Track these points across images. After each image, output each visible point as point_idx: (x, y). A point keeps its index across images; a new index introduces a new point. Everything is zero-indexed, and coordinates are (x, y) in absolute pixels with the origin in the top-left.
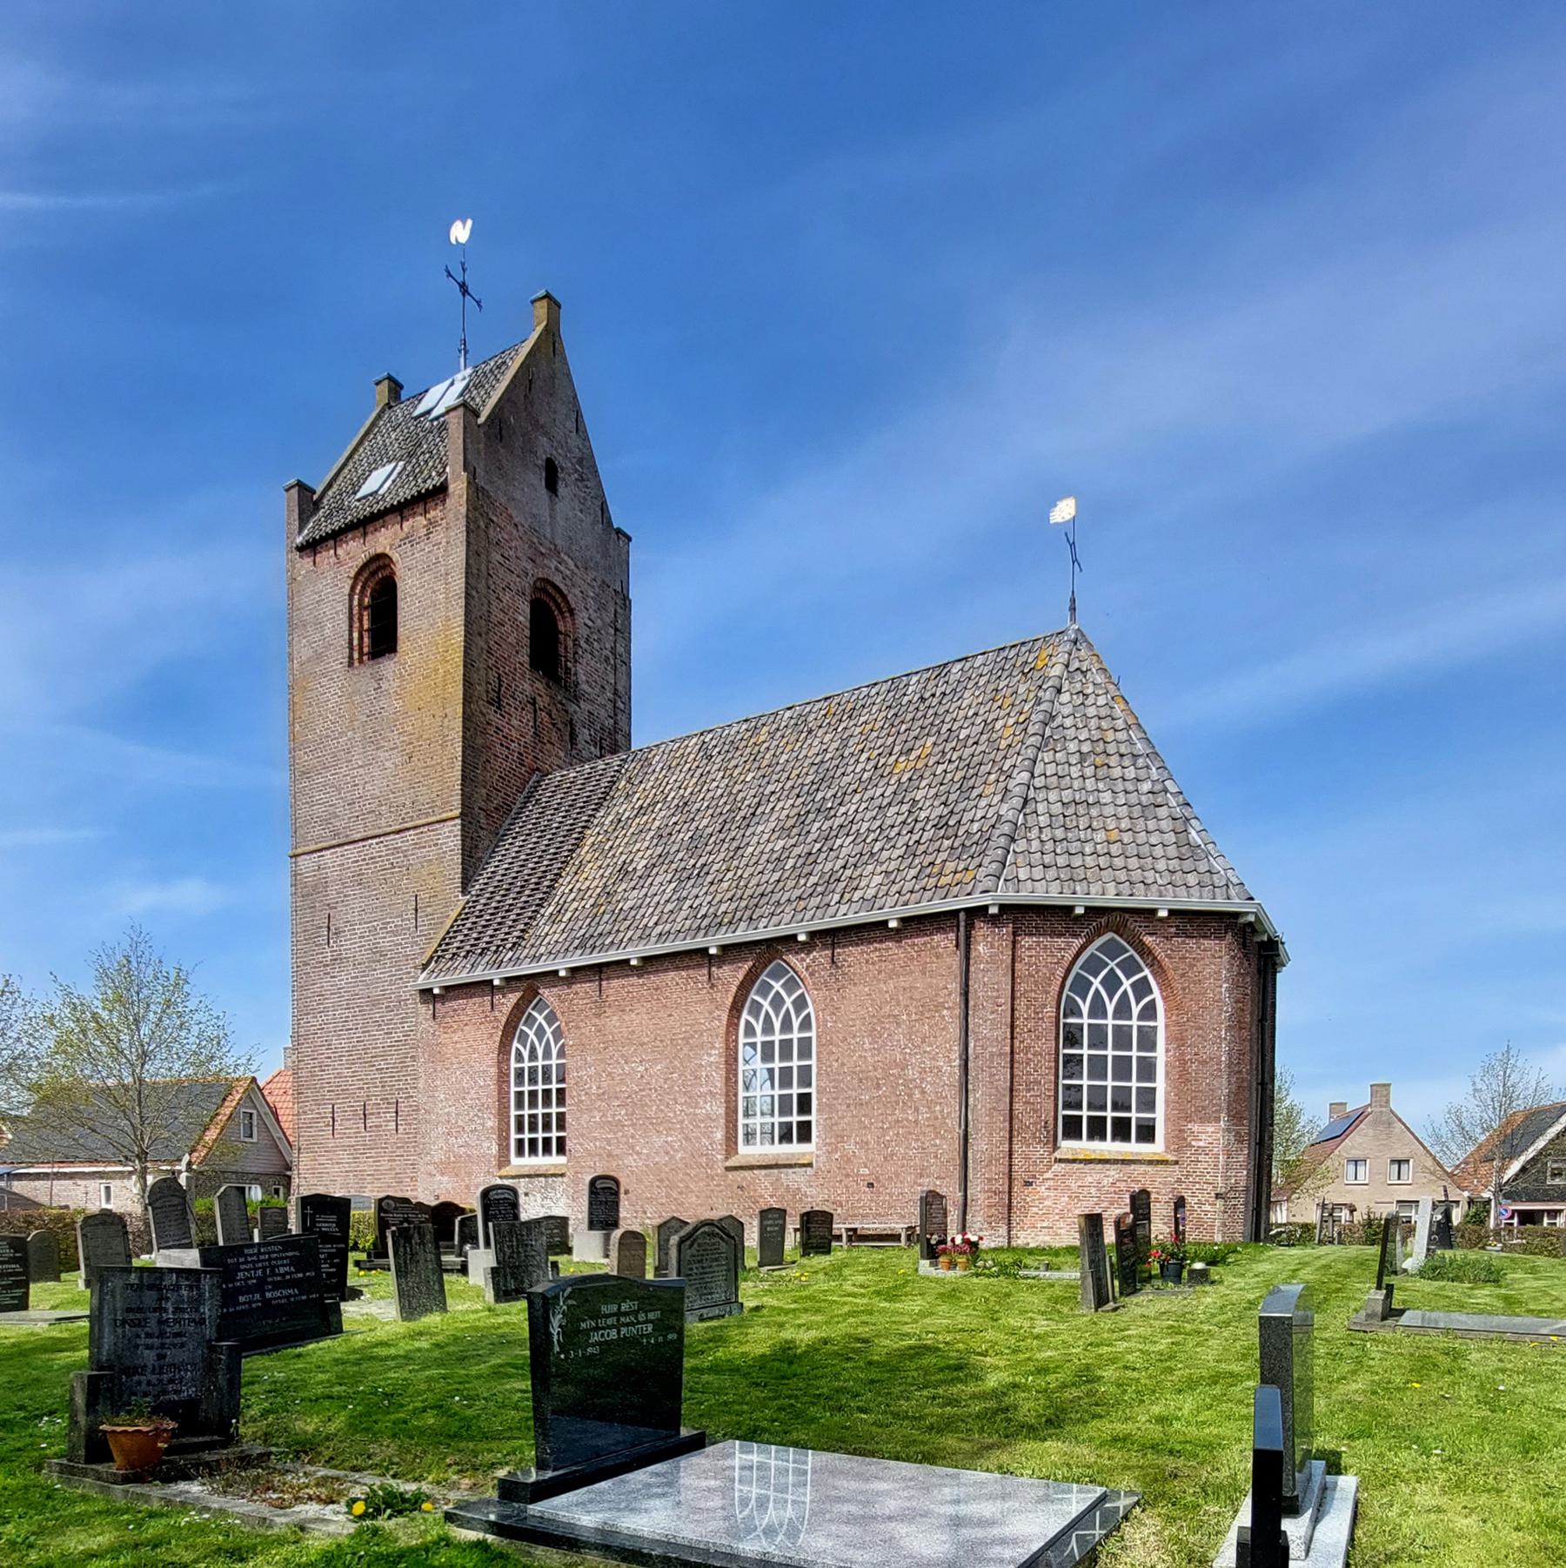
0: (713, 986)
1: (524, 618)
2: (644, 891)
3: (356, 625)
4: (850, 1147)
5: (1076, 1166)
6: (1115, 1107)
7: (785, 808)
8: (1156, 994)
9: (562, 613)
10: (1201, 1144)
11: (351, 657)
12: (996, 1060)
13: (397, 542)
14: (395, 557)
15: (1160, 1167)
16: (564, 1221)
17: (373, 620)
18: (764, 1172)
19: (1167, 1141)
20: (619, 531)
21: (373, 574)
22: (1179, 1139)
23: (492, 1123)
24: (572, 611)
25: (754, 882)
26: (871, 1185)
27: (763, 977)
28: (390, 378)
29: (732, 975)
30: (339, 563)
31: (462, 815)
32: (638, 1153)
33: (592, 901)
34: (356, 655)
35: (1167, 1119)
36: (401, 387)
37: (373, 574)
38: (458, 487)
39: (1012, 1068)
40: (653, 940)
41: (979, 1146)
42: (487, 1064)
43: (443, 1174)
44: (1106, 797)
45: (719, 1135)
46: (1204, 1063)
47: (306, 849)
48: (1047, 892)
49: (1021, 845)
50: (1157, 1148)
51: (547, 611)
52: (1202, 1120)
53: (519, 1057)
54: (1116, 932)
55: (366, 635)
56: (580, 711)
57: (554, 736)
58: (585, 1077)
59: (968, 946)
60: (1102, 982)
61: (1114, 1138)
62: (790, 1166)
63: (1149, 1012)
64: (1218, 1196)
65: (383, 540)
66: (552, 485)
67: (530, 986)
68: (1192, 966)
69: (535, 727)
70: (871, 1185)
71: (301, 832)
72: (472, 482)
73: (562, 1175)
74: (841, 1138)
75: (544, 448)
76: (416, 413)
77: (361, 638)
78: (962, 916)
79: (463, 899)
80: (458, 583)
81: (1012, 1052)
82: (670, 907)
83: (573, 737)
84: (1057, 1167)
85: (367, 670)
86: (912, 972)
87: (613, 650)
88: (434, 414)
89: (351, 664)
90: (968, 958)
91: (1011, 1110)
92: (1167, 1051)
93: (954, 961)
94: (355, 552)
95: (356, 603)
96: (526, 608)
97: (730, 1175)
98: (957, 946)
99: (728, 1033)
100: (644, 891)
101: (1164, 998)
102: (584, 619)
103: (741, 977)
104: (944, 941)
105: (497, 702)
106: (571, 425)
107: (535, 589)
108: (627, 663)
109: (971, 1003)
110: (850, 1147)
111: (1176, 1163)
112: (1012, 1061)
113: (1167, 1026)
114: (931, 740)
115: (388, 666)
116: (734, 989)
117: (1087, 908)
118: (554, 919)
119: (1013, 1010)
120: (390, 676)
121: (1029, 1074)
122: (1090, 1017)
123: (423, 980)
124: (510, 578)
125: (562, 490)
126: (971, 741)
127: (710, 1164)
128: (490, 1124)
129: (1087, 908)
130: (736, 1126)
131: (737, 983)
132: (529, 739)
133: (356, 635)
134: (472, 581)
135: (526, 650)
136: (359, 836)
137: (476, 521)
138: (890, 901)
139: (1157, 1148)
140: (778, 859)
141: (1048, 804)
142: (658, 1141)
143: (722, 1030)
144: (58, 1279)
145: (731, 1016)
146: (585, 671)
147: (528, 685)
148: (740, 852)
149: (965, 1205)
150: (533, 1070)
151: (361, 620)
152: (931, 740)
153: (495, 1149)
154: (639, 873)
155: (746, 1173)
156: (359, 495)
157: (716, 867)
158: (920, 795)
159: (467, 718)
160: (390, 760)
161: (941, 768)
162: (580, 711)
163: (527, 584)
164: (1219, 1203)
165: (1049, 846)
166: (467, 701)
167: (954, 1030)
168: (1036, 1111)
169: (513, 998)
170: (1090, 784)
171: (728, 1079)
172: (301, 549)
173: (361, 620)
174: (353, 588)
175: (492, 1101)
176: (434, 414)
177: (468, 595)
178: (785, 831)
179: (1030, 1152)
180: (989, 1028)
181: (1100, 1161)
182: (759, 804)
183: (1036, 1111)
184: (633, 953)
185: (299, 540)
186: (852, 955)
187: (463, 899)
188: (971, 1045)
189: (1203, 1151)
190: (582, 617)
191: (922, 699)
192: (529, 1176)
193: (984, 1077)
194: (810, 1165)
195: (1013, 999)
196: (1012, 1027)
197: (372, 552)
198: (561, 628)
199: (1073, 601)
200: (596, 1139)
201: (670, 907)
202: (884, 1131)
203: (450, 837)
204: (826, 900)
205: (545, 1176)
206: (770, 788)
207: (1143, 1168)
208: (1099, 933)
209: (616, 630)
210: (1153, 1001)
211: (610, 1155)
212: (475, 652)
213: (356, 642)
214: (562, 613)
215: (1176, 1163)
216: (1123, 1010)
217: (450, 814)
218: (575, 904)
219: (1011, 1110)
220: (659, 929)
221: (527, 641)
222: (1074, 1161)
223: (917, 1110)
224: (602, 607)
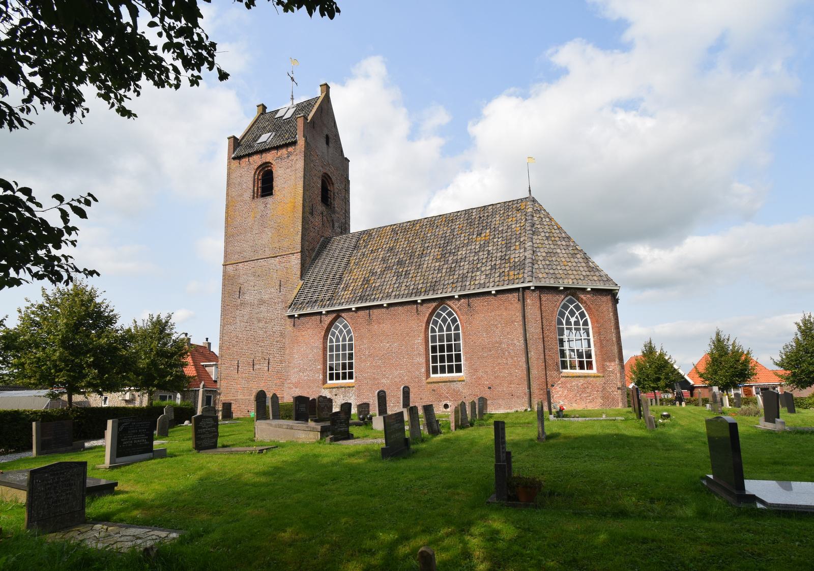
0: (418, 314)
1: (319, 185)
2: (383, 280)
3: (256, 185)
4: (480, 373)
5: (569, 379)
6: (336, 370)
7: (436, 252)
8: (587, 316)
9: (329, 184)
10: (611, 369)
11: (254, 196)
12: (538, 340)
13: (275, 158)
14: (274, 163)
15: (597, 379)
16: (350, 404)
17: (263, 183)
18: (443, 384)
19: (597, 369)
20: (346, 158)
21: (263, 169)
22: (602, 368)
23: (320, 367)
24: (333, 184)
25: (430, 277)
26: (490, 388)
27: (438, 311)
28: (263, 105)
29: (427, 309)
30: (250, 164)
31: (301, 252)
32: (387, 378)
33: (360, 283)
34: (256, 195)
35: (597, 361)
36: (266, 108)
37: (263, 169)
38: (301, 142)
39: (544, 343)
40: (393, 297)
41: (534, 372)
42: (319, 343)
43: (296, 388)
44: (559, 251)
45: (423, 370)
46: (607, 341)
47: (231, 263)
48: (550, 283)
49: (536, 266)
50: (594, 371)
51: (326, 181)
52: (610, 361)
53: (331, 341)
54: (572, 296)
55: (259, 188)
56: (335, 216)
57: (328, 225)
58: (361, 349)
59: (524, 299)
60: (568, 313)
61: (587, 369)
62: (455, 381)
63: (457, 328)
64: (618, 388)
65: (269, 157)
66: (327, 143)
67: (338, 314)
68: (599, 307)
69: (322, 221)
70: (490, 388)
71: (228, 256)
72: (306, 141)
73: (353, 387)
74: (476, 370)
75: (326, 132)
76: (276, 117)
77: (258, 190)
78: (521, 289)
79: (301, 282)
80: (301, 174)
81: (543, 338)
82: (396, 286)
83: (333, 225)
84: (563, 379)
85: (262, 200)
86: (501, 309)
87: (345, 196)
88: (284, 118)
89: (253, 198)
90: (524, 305)
91: (545, 358)
92: (594, 337)
93: (519, 306)
94: (257, 160)
95: (256, 177)
96: (320, 182)
97: (429, 386)
98: (519, 300)
99: (425, 331)
100: (383, 280)
101: (590, 318)
102: (337, 186)
103: (430, 311)
104: (513, 297)
105: (312, 214)
106: (333, 125)
107: (322, 176)
108: (349, 201)
109: (526, 320)
110: (480, 373)
111: (603, 377)
112: (544, 341)
113: (593, 328)
114: (488, 231)
115: (269, 199)
116: (427, 315)
117: (564, 287)
118: (345, 289)
119: (542, 322)
120: (271, 203)
121: (549, 345)
122: (583, 325)
123: (289, 312)
124: (316, 172)
125: (330, 145)
126: (504, 232)
127: (420, 381)
128: (319, 367)
129: (564, 287)
130: (429, 366)
131: (429, 313)
132: (321, 226)
133: (256, 188)
134: (306, 173)
135: (320, 196)
136: (255, 258)
137: (307, 153)
138: (492, 284)
139: (594, 371)
140: (438, 269)
141: (541, 254)
142: (396, 373)
143: (423, 330)
144: (806, 389)
145: (426, 325)
146: (337, 203)
147: (320, 207)
148: (421, 267)
149: (530, 395)
150: (338, 346)
151: (258, 183)
152: (488, 231)
153: (321, 377)
154: (378, 273)
155: (436, 385)
156: (258, 142)
157: (412, 272)
158: (490, 248)
159: (303, 218)
160: (269, 234)
161: (495, 240)
162: (335, 216)
163: (320, 174)
164: (619, 391)
165: (545, 266)
166: (303, 212)
167: (521, 331)
168: (552, 359)
169: (331, 317)
170: (552, 246)
171: (426, 349)
172: (234, 158)
173: (258, 183)
174: (255, 173)
175: (321, 358)
176: (284, 118)
177: (304, 177)
178: (438, 260)
179: (552, 373)
180: (534, 329)
181: (577, 377)
182: (424, 250)
183: (552, 359)
184: (385, 303)
185: (233, 156)
186: (475, 302)
187: (301, 282)
188: (528, 335)
189: (612, 372)
190: (336, 186)
191: (480, 217)
192: (337, 388)
193: (534, 346)
194: (463, 381)
195: (542, 319)
196: (542, 328)
197: (264, 161)
198: (329, 188)
199: (530, 187)
200: (368, 372)
201: (396, 286)
202: (494, 368)
203: (295, 261)
204: (464, 284)
205: (345, 387)
206: (427, 245)
207: (592, 379)
208: (567, 296)
209: (345, 190)
210: (587, 319)
211: (374, 378)
212: (306, 196)
213: (256, 191)
214: (329, 184)
215: (603, 377)
216: (449, 329)
217: (296, 251)
218: (353, 284)
219: (545, 358)
220: (394, 294)
221: (320, 193)
222: (568, 377)
223: (507, 359)
224: (341, 183)
